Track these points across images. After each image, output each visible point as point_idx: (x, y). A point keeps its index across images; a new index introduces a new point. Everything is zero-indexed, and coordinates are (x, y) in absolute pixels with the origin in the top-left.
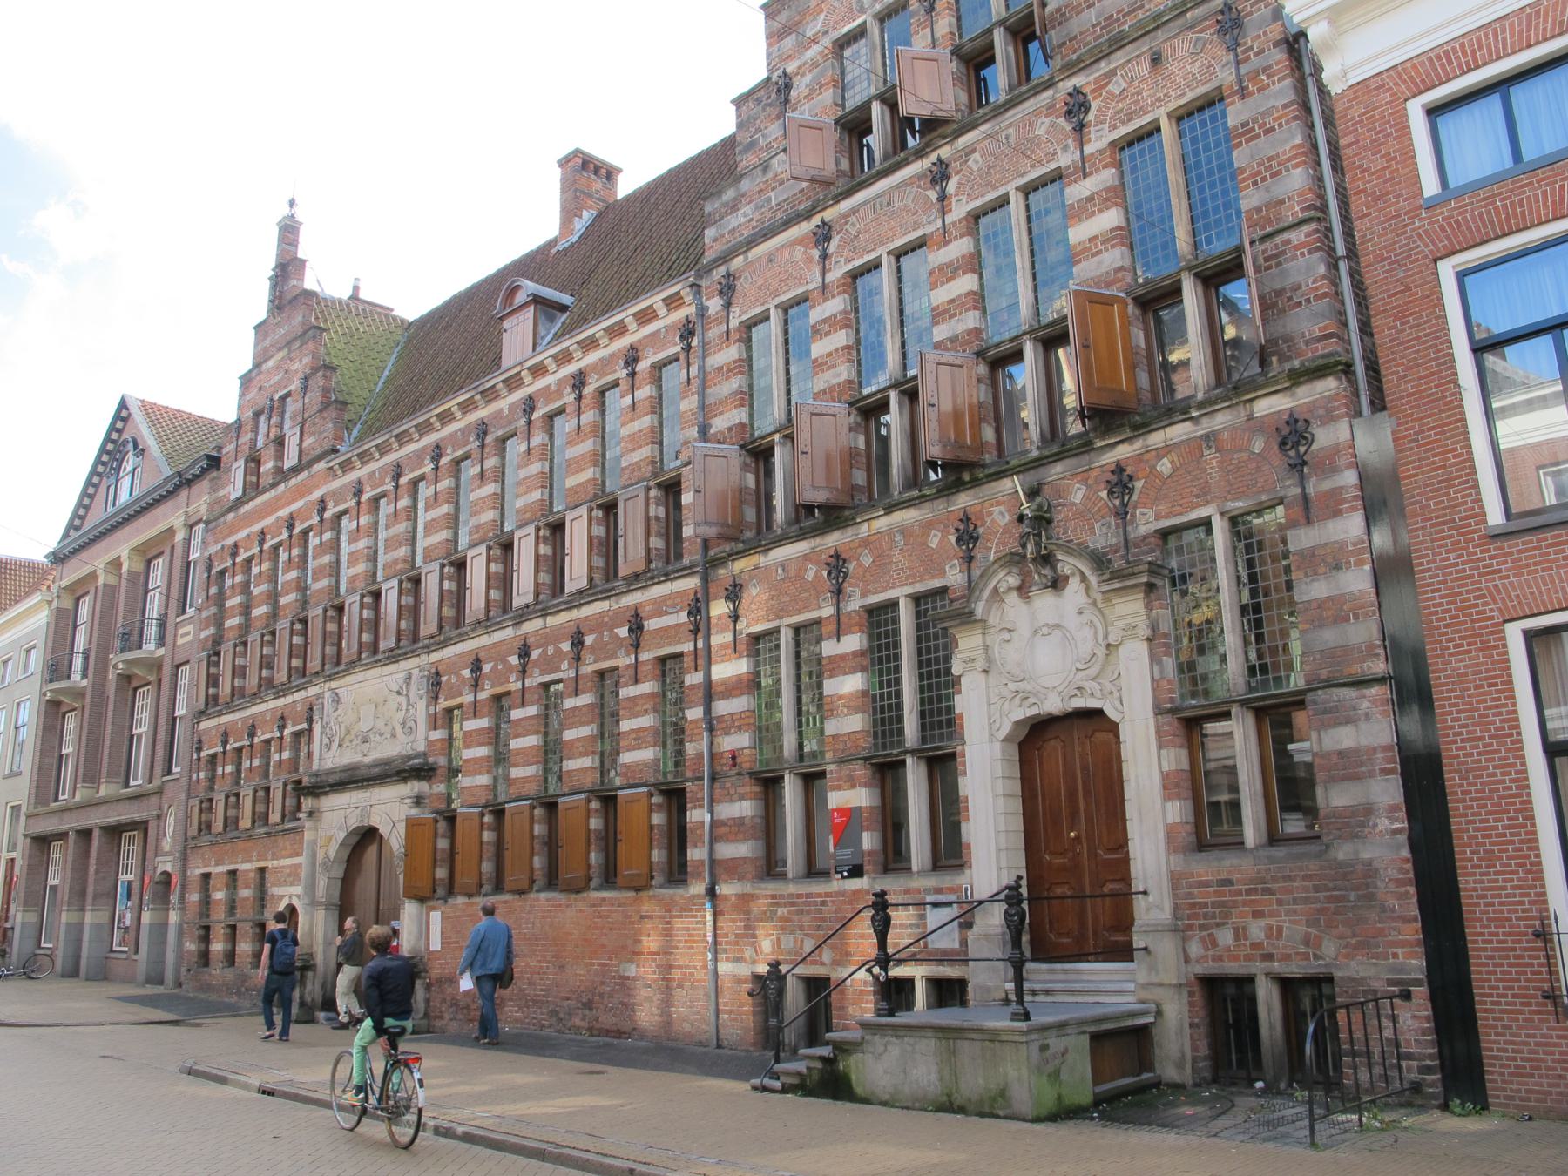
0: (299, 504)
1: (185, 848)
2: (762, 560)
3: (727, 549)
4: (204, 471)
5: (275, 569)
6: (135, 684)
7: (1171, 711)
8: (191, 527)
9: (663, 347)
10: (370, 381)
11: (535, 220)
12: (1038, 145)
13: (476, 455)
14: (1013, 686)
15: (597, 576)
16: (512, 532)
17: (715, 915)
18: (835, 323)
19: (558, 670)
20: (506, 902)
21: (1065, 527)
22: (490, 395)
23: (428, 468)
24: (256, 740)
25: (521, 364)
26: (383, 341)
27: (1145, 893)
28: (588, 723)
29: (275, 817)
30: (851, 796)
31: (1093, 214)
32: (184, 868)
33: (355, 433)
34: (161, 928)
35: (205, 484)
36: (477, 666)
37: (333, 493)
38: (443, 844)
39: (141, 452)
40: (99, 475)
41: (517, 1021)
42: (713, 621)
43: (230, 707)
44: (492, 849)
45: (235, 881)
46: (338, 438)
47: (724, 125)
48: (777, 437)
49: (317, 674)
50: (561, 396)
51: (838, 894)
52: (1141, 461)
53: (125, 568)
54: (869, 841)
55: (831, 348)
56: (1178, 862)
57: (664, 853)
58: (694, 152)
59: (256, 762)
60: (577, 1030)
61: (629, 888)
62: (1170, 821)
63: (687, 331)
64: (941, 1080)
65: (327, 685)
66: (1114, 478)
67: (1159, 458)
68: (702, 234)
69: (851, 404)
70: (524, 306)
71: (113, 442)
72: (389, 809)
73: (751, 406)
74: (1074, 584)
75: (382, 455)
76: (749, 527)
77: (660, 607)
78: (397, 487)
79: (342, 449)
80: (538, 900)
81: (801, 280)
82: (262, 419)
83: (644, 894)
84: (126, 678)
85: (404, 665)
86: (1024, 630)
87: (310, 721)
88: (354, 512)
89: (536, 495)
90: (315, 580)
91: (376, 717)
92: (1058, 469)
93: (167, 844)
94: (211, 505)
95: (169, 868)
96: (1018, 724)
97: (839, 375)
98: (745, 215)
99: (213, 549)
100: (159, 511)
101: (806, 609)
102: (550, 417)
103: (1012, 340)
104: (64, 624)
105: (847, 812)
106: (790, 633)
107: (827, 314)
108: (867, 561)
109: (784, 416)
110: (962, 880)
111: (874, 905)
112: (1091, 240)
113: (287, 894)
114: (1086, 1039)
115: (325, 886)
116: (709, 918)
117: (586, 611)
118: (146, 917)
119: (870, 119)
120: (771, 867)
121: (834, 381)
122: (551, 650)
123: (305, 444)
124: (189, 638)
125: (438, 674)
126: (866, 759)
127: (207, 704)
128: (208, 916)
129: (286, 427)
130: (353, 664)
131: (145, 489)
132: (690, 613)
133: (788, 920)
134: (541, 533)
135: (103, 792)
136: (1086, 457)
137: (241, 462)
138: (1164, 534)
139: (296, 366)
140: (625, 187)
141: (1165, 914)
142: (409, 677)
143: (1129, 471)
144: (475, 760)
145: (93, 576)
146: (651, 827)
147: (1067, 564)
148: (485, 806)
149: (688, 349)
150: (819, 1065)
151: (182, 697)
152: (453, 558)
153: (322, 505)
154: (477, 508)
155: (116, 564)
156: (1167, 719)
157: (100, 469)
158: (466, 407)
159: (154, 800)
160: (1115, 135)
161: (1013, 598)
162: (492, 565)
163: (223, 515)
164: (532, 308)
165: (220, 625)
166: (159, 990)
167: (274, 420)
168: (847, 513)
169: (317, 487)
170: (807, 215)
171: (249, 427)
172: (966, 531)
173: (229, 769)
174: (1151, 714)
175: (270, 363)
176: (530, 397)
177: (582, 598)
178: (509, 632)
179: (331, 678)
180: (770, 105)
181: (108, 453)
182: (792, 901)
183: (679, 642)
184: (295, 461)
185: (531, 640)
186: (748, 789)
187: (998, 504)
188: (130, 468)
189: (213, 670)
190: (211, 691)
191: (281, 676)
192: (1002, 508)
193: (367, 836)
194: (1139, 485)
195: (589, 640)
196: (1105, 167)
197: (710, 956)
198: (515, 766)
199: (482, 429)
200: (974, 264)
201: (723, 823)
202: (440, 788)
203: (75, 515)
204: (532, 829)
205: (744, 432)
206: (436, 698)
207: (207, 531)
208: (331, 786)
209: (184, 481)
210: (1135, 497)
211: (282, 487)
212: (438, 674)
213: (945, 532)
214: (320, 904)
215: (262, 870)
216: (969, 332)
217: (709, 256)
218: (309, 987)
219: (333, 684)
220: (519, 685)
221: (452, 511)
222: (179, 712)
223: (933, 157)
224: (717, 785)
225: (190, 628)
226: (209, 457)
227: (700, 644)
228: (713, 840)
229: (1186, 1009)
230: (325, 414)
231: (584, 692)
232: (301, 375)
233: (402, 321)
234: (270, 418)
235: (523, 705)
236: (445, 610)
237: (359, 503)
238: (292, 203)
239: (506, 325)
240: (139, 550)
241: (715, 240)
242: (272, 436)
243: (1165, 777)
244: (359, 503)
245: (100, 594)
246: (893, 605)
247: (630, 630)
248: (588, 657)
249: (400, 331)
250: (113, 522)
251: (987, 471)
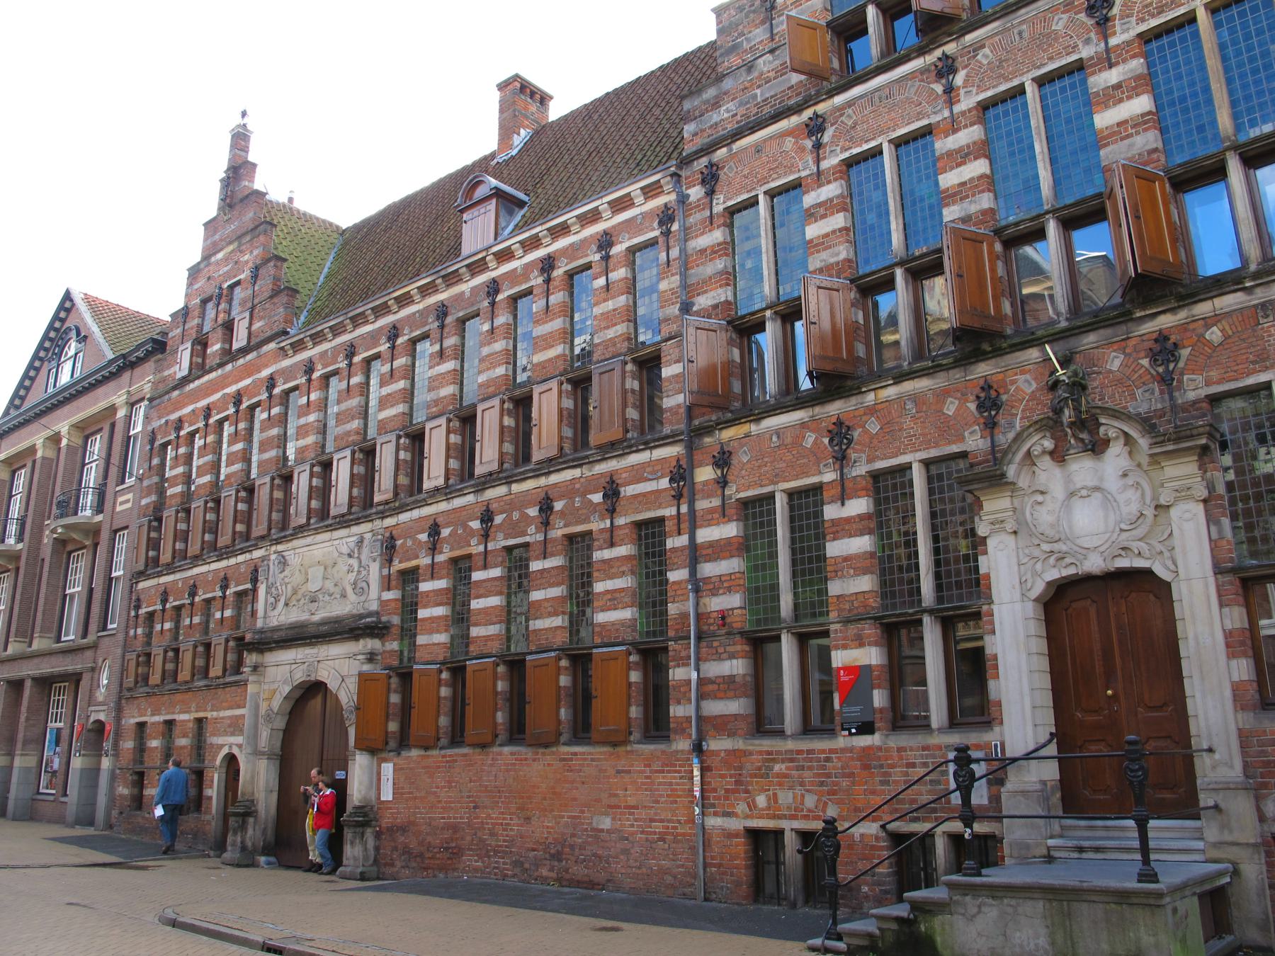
0: (248, 382)
1: (120, 698)
2: (754, 428)
3: (714, 418)
4: (149, 355)
5: (220, 442)
6: (69, 548)
7: (1232, 571)
8: (133, 405)
9: (640, 231)
10: (312, 277)
11: (473, 136)
12: (1056, 39)
13: (435, 334)
14: (1046, 547)
15: (567, 447)
16: (474, 406)
17: (703, 770)
18: (831, 207)
19: (524, 534)
20: (465, 755)
21: (1100, 392)
22: (452, 279)
23: (384, 347)
25: (487, 249)
26: (321, 243)
27: (1210, 750)
28: (558, 584)
29: (216, 671)
30: (858, 655)
31: (1121, 101)
32: (118, 719)
33: (302, 318)
34: (92, 774)
35: (150, 365)
36: (435, 530)
37: (282, 372)
38: (395, 698)
39: (83, 339)
40: (41, 360)
41: (476, 870)
42: (698, 487)
43: (170, 568)
44: (449, 704)
45: (170, 730)
46: (288, 321)
47: (703, 32)
48: (768, 313)
49: (263, 538)
50: (528, 279)
51: (843, 750)
52: (1186, 330)
53: (64, 442)
54: (879, 698)
55: (828, 229)
56: (1248, 720)
57: (641, 709)
58: (599, 93)
59: (196, 620)
60: (545, 880)
61: (603, 743)
62: (1236, 678)
63: (666, 217)
64: (1053, 943)
65: (274, 548)
66: (1157, 347)
67: (1208, 327)
69: (852, 281)
70: (486, 199)
71: (57, 330)
72: (339, 667)
73: (735, 285)
74: (1116, 450)
75: (335, 336)
76: (727, 399)
77: (638, 474)
78: (350, 365)
79: (292, 332)
80: (500, 754)
81: (791, 168)
82: (210, 305)
83: (621, 749)
84: (61, 543)
85: (355, 529)
86: (1058, 490)
87: (255, 581)
88: (305, 389)
89: (501, 371)
90: (198, 476)
91: (325, 578)
92: (1091, 339)
93: (101, 694)
94: (155, 384)
95: (102, 717)
96: (1049, 583)
97: (838, 254)
98: (728, 111)
99: (156, 424)
100: (100, 391)
101: (807, 475)
102: (514, 299)
103: (1032, 219)
105: (855, 671)
106: (785, 499)
107: (823, 198)
108: (874, 427)
109: (774, 294)
110: (992, 737)
111: (956, 760)
112: (1119, 124)
113: (225, 743)
114: (1195, 899)
115: (267, 737)
116: (696, 773)
117: (554, 478)
118: (77, 763)
119: (865, 21)
120: (763, 722)
121: (833, 260)
122: (516, 515)
123: (254, 327)
124: (129, 505)
125: (392, 538)
126: (875, 619)
127: (147, 565)
128: (142, 762)
129: (233, 313)
130: (301, 530)
131: (87, 371)
132: (670, 481)
133: (786, 776)
134: (506, 406)
135: (36, 645)
136: (1124, 328)
137: (189, 345)
138: (1215, 400)
140: (556, 111)
141: (1235, 772)
142: (360, 542)
143: (1173, 338)
144: (432, 619)
145: (32, 450)
146: (630, 684)
147: (1110, 427)
148: (442, 663)
149: (667, 234)
150: (894, 926)
151: (120, 558)
152: (409, 430)
153: (309, 368)
154: (436, 384)
155: (55, 439)
156: (1228, 578)
157: (42, 354)
158: (425, 291)
159: (89, 653)
160: (1143, 27)
161: (1046, 462)
162: (314, 480)
163: (167, 393)
164: (494, 201)
165: (161, 492)
166: (90, 831)
167: (223, 306)
168: (849, 383)
169: (267, 366)
170: (798, 109)
171: (196, 313)
172: (988, 397)
173: (167, 626)
174: (1211, 573)
175: (220, 256)
176: (494, 281)
177: (550, 465)
178: (470, 498)
179: (278, 541)
180: (754, 12)
181: (51, 340)
182: (790, 757)
183: (659, 507)
184: (244, 343)
185: (494, 506)
186: (739, 648)
187: (1023, 376)
188: (72, 352)
189: (153, 535)
190: (151, 553)
191: (166, 557)
192: (1028, 377)
193: (313, 690)
194: (1185, 353)
195: (558, 506)
196: (1133, 57)
197: (697, 810)
198: (476, 625)
199: (442, 311)
200: (728, 248)
201: (711, 681)
203: (16, 395)
204: (495, 685)
205: (730, 310)
206: (390, 561)
207: (149, 408)
208: (277, 642)
209: (126, 364)
210: (1181, 364)
211: (229, 367)
212: (392, 538)
213: (963, 399)
214: (263, 754)
215: (200, 721)
216: (984, 212)
217: (688, 149)
218: (250, 832)
219: (280, 548)
220: (481, 548)
221: (408, 386)
223: (938, 53)
224: (704, 644)
225: (130, 496)
226: (154, 341)
227: (684, 509)
228: (701, 696)
229: (1264, 868)
230: (275, 300)
231: (553, 555)
232: (251, 264)
233: (337, 227)
234: (218, 304)
235: (485, 567)
236: (451, 461)
237: (309, 380)
238: (244, 114)
239: (465, 217)
240: (77, 427)
241: (695, 134)
242: (220, 321)
243: (1228, 635)
244: (309, 380)
245: (38, 466)
246: (908, 467)
247: (541, 510)
248: (557, 522)
249: (336, 236)
250: (54, 401)
251: (1010, 342)
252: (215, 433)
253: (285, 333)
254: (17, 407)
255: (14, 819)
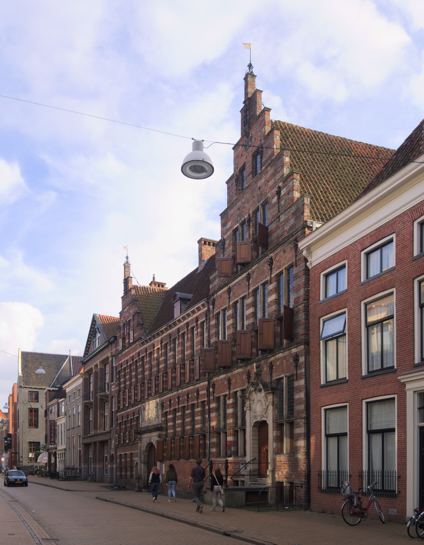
0: (134, 353)
6: (104, 401)
22: (171, 327)
24: (129, 419)
28: (189, 418)
32: (116, 453)
68: (209, 286)
93: (113, 446)
104: (86, 383)
123: (135, 335)
124: (114, 389)
137: (121, 340)
139: (131, 312)
145: (91, 369)
158: (166, 329)
161: (254, 393)
165: (120, 386)
169: (138, 349)
175: (126, 310)
189: (142, 389)
193: (151, 445)
194: (274, 367)
202: (164, 433)
211: (130, 348)
214: (142, 462)
218: (141, 483)
222: (113, 410)
225: (114, 386)
232: (132, 315)
238: (127, 258)
246: (282, 378)
252: (141, 361)
253: (141, 338)
254: (87, 354)
255: (98, 482)
